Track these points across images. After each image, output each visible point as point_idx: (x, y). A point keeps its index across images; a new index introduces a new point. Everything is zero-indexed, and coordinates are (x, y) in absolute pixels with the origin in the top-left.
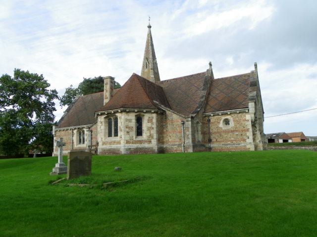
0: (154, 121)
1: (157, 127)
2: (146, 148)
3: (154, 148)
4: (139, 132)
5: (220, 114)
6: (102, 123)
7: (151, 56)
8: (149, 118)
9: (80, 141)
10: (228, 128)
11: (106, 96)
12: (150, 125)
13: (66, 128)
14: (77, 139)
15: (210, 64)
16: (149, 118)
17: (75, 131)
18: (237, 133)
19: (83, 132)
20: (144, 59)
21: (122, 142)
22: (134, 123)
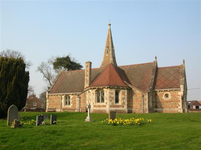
0: (126, 94)
1: (127, 98)
2: (118, 110)
3: (107, 111)
4: (117, 101)
5: (163, 91)
6: (93, 94)
7: (110, 45)
8: (123, 92)
9: (66, 103)
11: (87, 74)
12: (123, 96)
13: (56, 94)
14: (64, 102)
16: (123, 92)
17: (63, 97)
18: (173, 103)
19: (69, 97)
20: (106, 47)
21: (108, 106)
22: (115, 95)
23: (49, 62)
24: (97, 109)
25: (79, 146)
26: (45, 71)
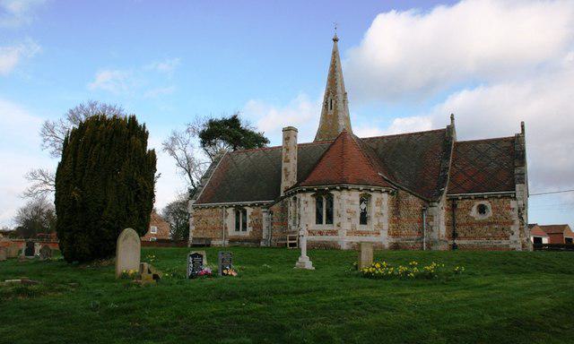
9: (237, 228)
10: (488, 216)
15: (452, 118)
19: (245, 213)
23: (188, 131)
24: (317, 238)
25: (434, 248)
26: (179, 153)
